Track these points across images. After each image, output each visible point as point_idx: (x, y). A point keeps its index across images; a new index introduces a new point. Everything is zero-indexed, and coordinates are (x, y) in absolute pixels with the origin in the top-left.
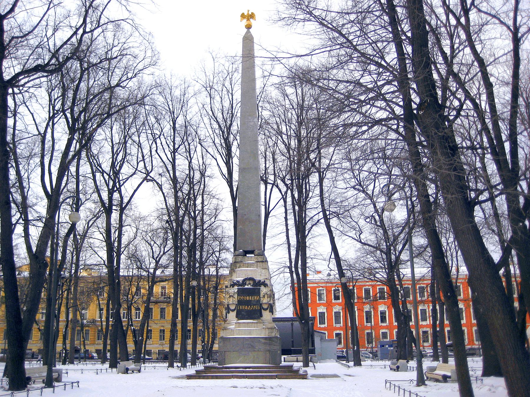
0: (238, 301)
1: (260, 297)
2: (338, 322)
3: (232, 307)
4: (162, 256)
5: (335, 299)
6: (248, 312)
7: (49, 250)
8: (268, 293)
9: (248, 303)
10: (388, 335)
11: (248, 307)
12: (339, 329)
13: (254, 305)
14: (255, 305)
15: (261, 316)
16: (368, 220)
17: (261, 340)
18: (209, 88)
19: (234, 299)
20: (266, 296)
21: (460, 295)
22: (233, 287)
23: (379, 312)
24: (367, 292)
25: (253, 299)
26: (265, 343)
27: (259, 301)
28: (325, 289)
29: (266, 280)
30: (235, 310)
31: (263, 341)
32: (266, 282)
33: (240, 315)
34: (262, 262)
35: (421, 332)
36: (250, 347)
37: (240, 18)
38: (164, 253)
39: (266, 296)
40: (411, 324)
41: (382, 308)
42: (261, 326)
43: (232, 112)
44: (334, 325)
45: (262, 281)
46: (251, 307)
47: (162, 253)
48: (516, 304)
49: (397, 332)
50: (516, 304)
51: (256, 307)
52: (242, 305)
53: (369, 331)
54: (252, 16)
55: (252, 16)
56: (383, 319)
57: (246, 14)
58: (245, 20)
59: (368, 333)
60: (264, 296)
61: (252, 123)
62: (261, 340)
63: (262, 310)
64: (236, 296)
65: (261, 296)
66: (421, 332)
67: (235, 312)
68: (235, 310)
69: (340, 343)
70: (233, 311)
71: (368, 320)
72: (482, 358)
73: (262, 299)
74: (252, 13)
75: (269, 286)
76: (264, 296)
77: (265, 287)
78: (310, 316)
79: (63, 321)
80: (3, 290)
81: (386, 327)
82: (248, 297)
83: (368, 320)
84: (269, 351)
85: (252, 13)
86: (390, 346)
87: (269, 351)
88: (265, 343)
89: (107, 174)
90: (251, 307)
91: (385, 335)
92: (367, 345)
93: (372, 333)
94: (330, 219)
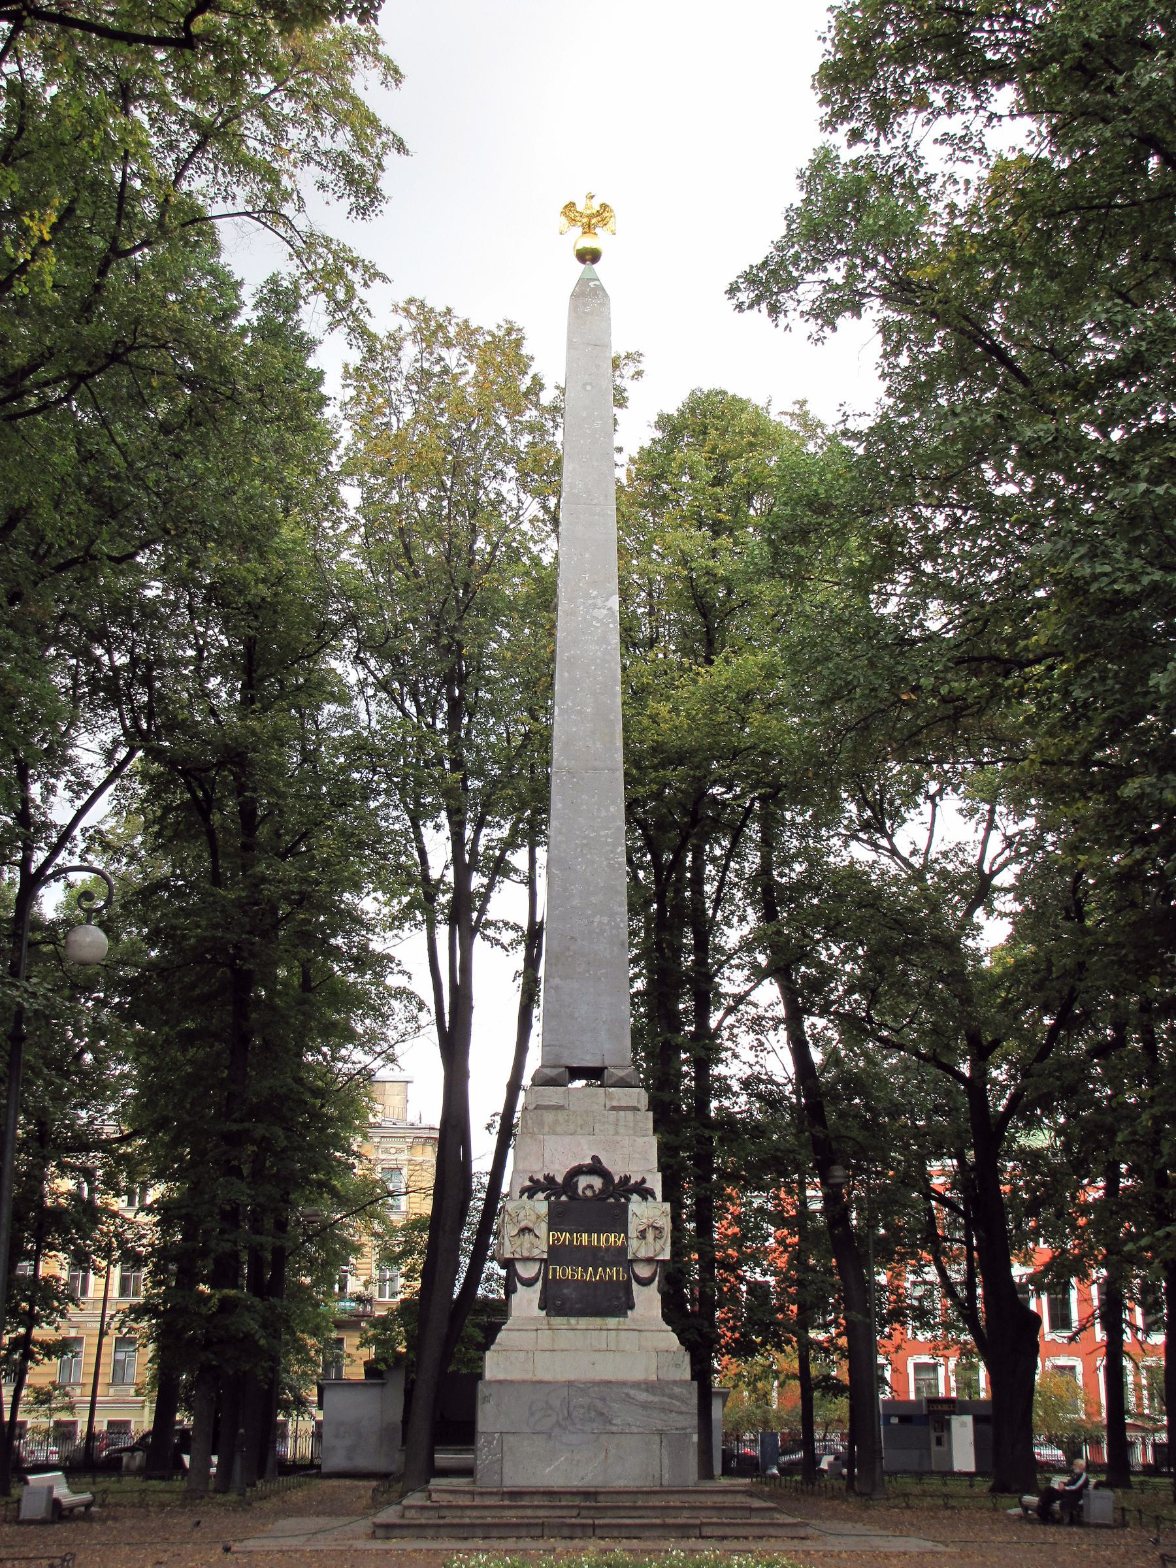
0: (552, 1249)
1: (626, 1236)
3: (526, 1271)
9: (593, 1257)
25: (603, 1243)
27: (623, 1249)
29: (648, 1178)
33: (555, 1302)
36: (591, 1420)
39: (650, 1235)
48: (467, 857)
50: (467, 857)
51: (614, 1273)
54: (598, 218)
55: (598, 218)
60: (643, 1235)
63: (635, 1285)
64: (542, 1229)
68: (536, 1279)
70: (529, 1283)
74: (604, 207)
76: (643, 1235)
77: (645, 1198)
78: (30, 1477)
79: (95, 1300)
82: (585, 1236)
84: (661, 1433)
89: (747, 993)
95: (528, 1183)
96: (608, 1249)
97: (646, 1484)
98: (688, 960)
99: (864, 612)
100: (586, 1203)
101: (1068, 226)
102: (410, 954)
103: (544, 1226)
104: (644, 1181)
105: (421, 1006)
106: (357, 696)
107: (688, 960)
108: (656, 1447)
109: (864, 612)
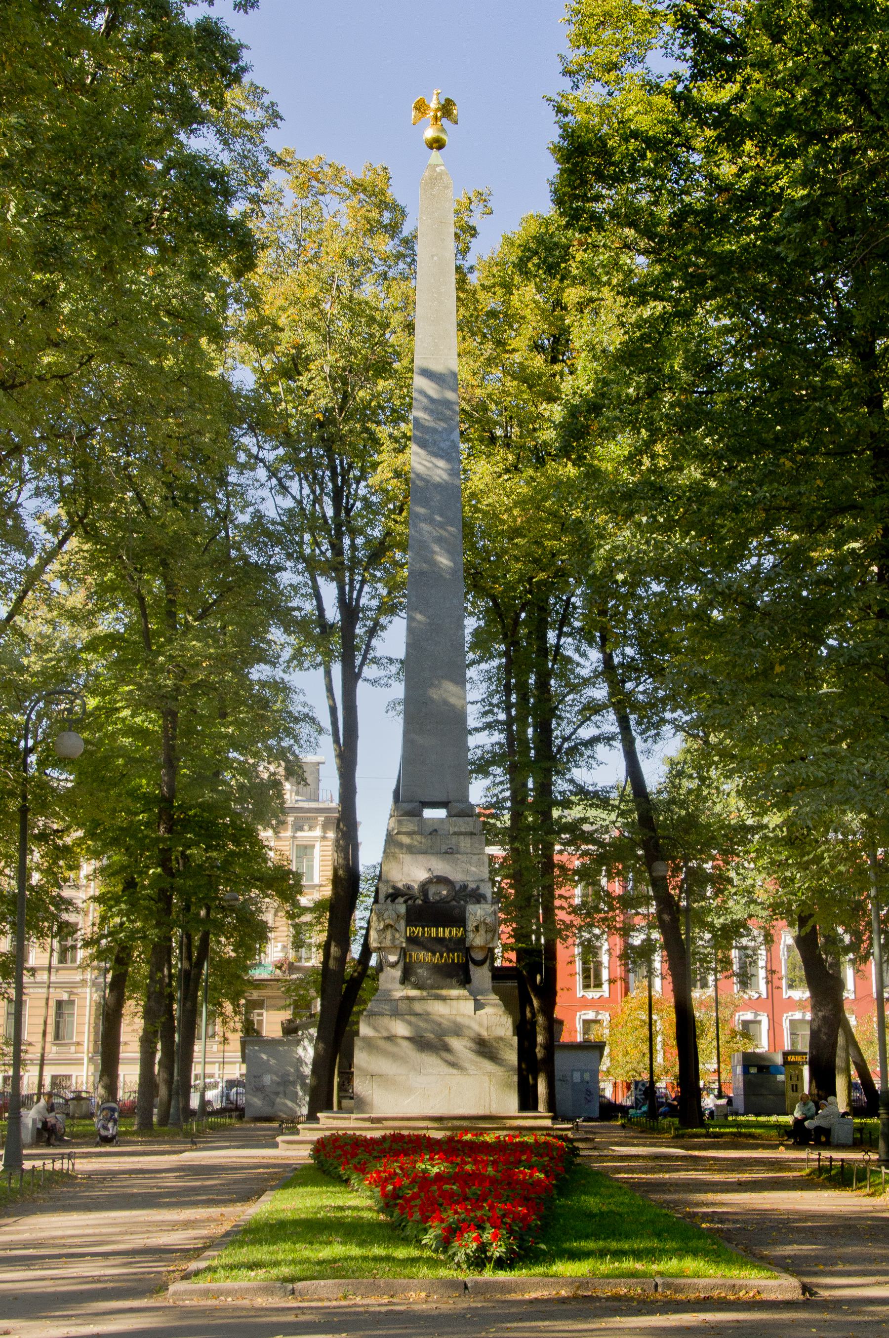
1: (465, 930)
7: (176, 1014)
8: (488, 920)
12: (586, 1004)
20: (482, 931)
22: (393, 901)
25: (447, 934)
27: (462, 940)
29: (482, 885)
32: (482, 891)
35: (786, 1025)
39: (482, 931)
43: (125, 1133)
45: (472, 886)
66: (786, 1025)
68: (397, 963)
72: (10, 936)
73: (471, 935)
76: (477, 928)
80: (313, 1031)
82: (434, 930)
95: (391, 891)
96: (451, 939)
97: (481, 1112)
98: (513, 698)
99: (714, 94)
100: (431, 912)
101: (868, 897)
102: (310, 688)
103: (403, 923)
104: (478, 888)
105: (320, 731)
106: (263, 492)
107: (513, 698)
108: (487, 1084)
109: (714, 94)
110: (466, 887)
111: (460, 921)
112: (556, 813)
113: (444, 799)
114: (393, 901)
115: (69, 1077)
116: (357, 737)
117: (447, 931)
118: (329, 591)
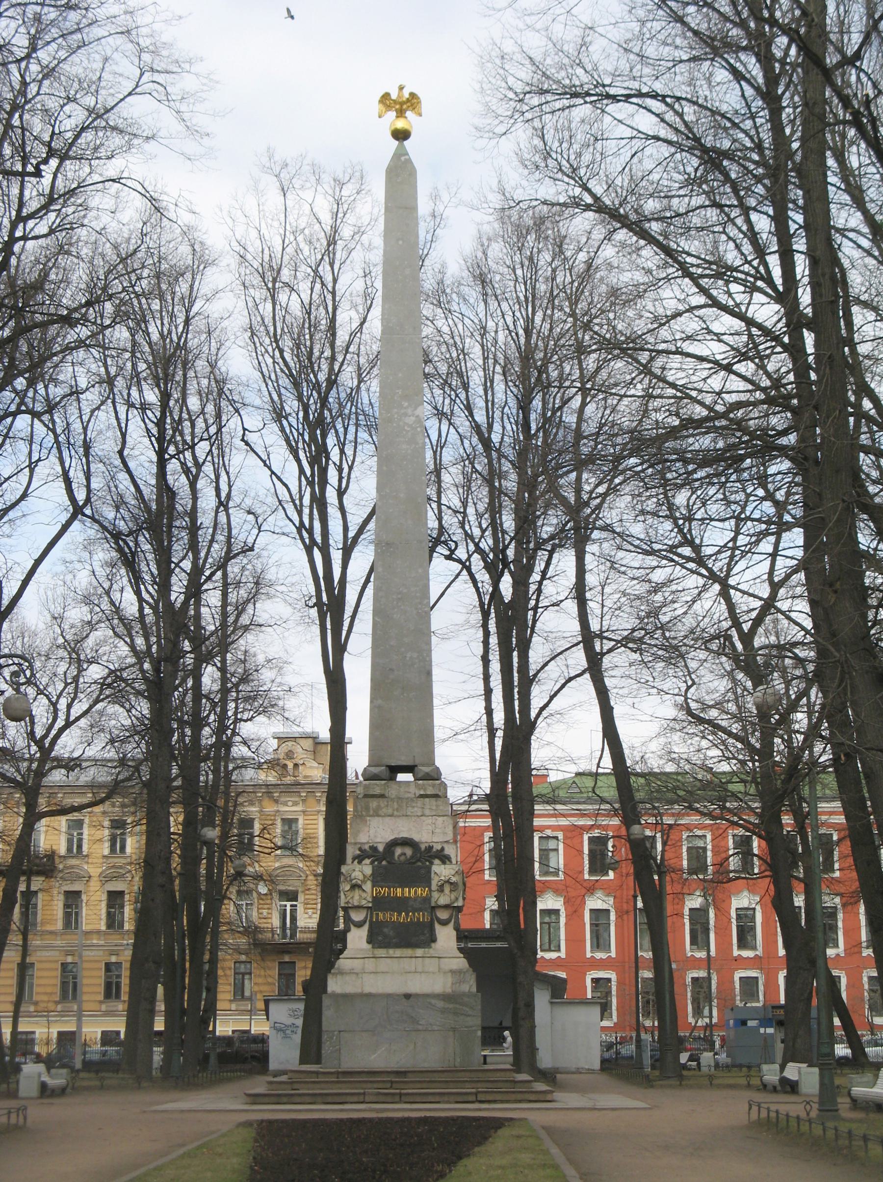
1: (430, 890)
2: (599, 942)
3: (357, 916)
4: (61, 731)
5: (592, 872)
6: (399, 928)
9: (401, 904)
10: (761, 988)
11: (400, 915)
12: (695, 963)
13: (414, 910)
14: (419, 910)
15: (434, 940)
16: (714, 646)
17: (433, 1001)
18: (271, 278)
19: (364, 895)
20: (447, 889)
21: (871, 978)
22: (360, 863)
23: (733, 914)
24: (698, 855)
26: (443, 1011)
28: (560, 835)
29: (446, 846)
30: (364, 922)
31: (440, 1004)
32: (446, 852)
34: (436, 796)
37: (376, 107)
38: (68, 724)
39: (447, 889)
40: (830, 952)
41: (742, 900)
42: (431, 965)
44: (589, 955)
46: (407, 915)
47: (60, 723)
49: (787, 978)
51: (422, 917)
52: (384, 910)
53: (702, 974)
54: (411, 103)
56: (745, 936)
57: (394, 96)
58: (392, 114)
59: (695, 980)
61: (411, 420)
62: (433, 1001)
63: (437, 926)
64: (368, 887)
65: (434, 887)
67: (366, 927)
68: (364, 922)
69: (605, 1008)
70: (359, 925)
71: (699, 936)
73: (435, 895)
74: (413, 95)
75: (454, 861)
77: (444, 863)
81: (756, 962)
82: (399, 890)
83: (699, 936)
84: (454, 1030)
85: (413, 95)
86: (765, 1023)
87: (454, 1030)
88: (443, 1011)
90: (407, 915)
91: (749, 984)
92: (691, 1020)
93: (709, 979)
94: (603, 654)
104: (443, 849)
110: (431, 848)
111: (425, 879)
112: (23, 878)
113: (410, 763)
114: (360, 863)
115: (34, 1033)
116: (345, 709)
117: (413, 891)
118: (540, 479)
